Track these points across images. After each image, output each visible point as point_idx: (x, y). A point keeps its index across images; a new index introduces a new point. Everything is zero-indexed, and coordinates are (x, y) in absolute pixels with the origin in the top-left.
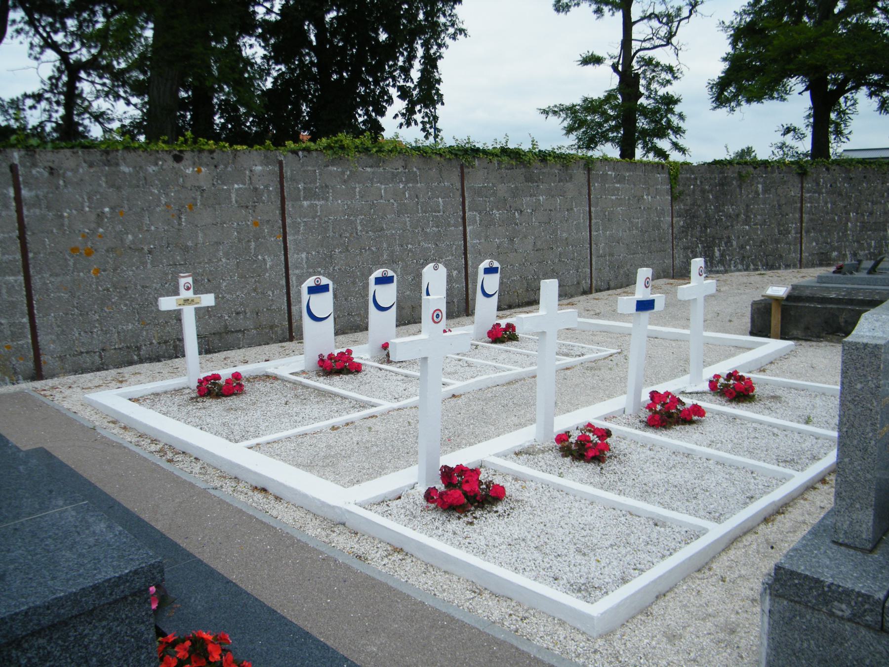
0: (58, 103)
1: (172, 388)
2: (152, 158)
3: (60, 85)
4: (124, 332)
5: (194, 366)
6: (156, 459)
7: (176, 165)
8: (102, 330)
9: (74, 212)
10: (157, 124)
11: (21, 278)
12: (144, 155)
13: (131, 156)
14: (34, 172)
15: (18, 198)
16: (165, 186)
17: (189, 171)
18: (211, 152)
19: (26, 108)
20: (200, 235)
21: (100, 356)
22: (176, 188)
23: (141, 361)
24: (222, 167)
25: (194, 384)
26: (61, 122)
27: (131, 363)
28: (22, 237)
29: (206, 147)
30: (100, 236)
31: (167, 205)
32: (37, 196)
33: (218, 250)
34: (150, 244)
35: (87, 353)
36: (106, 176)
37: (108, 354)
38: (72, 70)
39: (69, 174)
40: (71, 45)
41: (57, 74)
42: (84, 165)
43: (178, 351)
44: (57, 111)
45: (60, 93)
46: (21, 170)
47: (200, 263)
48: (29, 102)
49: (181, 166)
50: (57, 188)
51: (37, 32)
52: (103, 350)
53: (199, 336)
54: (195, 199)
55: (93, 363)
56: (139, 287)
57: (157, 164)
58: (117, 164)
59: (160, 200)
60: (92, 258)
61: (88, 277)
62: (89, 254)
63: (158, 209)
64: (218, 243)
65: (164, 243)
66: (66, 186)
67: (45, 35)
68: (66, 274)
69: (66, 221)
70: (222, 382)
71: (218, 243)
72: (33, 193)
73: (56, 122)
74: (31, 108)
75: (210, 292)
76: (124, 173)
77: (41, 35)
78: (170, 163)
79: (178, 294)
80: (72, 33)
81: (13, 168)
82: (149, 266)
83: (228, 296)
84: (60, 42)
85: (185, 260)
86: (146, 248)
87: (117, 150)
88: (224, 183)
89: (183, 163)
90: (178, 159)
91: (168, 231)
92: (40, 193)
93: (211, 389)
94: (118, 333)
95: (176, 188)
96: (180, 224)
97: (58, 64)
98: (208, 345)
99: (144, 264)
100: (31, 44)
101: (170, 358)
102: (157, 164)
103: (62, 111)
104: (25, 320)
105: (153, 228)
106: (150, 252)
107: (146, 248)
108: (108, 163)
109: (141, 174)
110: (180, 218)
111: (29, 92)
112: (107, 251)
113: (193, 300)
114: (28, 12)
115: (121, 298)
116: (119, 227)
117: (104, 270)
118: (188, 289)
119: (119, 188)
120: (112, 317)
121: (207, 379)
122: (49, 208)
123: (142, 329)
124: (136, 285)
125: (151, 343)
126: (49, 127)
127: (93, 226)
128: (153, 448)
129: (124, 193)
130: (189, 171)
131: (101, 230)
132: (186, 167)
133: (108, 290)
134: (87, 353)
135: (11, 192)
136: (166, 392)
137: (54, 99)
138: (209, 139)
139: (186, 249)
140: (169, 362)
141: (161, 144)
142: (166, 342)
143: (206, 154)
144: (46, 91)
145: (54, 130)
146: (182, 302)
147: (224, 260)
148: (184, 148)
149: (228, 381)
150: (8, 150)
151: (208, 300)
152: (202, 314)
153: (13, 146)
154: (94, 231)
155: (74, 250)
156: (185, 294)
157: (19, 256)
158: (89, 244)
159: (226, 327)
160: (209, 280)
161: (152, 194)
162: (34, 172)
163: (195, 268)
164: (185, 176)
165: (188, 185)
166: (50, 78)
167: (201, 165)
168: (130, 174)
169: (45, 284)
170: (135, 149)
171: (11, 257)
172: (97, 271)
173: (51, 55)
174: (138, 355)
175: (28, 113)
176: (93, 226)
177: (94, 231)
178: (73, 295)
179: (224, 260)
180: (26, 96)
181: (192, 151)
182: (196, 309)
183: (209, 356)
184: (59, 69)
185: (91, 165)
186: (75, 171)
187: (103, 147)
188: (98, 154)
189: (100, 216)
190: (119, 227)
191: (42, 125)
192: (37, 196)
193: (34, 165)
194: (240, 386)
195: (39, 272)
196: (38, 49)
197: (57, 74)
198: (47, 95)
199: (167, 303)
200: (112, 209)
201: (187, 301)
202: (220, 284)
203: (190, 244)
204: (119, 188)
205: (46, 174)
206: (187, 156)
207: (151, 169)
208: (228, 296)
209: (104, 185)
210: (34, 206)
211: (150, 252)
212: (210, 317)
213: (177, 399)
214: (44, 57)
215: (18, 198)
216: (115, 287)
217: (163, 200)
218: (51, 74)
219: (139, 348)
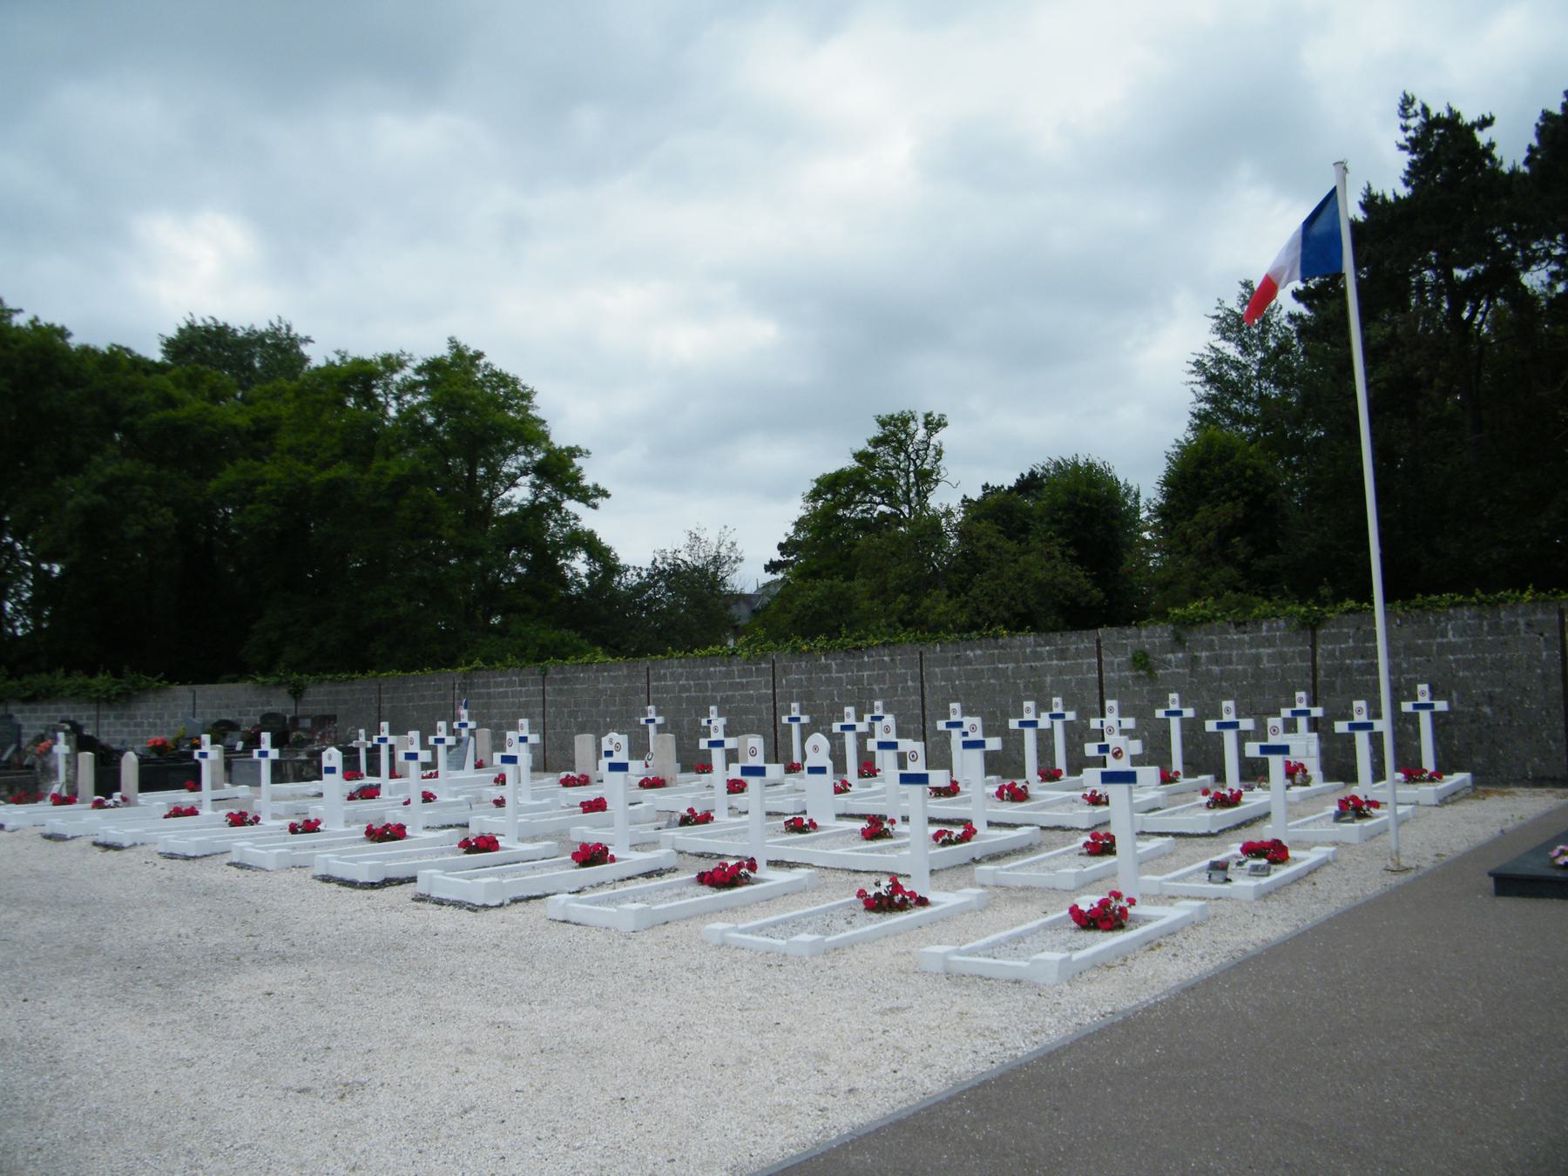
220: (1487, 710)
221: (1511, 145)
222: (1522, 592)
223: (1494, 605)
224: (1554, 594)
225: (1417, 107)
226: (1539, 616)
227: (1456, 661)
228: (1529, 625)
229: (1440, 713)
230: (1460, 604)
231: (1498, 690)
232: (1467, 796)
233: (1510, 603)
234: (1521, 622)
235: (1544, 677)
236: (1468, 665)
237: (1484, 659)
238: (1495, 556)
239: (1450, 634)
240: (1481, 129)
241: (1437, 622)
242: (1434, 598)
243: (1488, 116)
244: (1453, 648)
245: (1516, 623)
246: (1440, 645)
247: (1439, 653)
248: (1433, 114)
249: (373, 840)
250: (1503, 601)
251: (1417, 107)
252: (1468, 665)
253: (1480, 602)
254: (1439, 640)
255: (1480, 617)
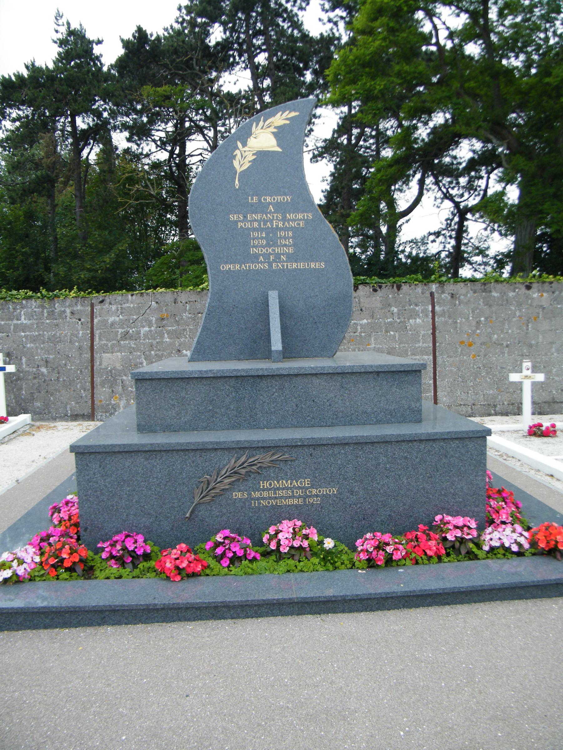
0: (451, 237)
1: (512, 429)
2: (512, 287)
3: (453, 223)
5: (528, 419)
6: (498, 458)
7: (527, 292)
9: (464, 320)
10: (521, 260)
11: (431, 357)
12: (507, 285)
13: (499, 286)
14: (443, 296)
15: (433, 311)
16: (519, 305)
17: (535, 295)
18: (551, 283)
19: (429, 242)
20: (540, 337)
21: (472, 408)
22: (527, 306)
23: (496, 414)
24: (557, 293)
25: (526, 428)
26: (452, 251)
27: (490, 415)
28: (434, 334)
29: (547, 280)
31: (520, 317)
32: (443, 310)
33: (551, 348)
34: (507, 341)
36: (483, 298)
37: (476, 407)
38: (462, 213)
39: (462, 297)
40: (462, 196)
41: (451, 217)
42: (471, 292)
43: (518, 411)
44: (449, 243)
45: (452, 230)
46: (436, 295)
48: (432, 238)
49: (530, 292)
50: (455, 305)
51: (440, 189)
53: (534, 403)
54: (538, 313)
56: (499, 368)
57: (514, 291)
58: (490, 291)
59: (515, 314)
60: (472, 348)
62: (470, 345)
63: (514, 319)
64: (552, 343)
65: (516, 341)
66: (459, 304)
67: (445, 190)
68: (456, 357)
69: (459, 325)
70: (543, 428)
71: (552, 343)
72: (441, 308)
73: (448, 251)
74: (432, 242)
76: (494, 297)
77: (443, 192)
78: (523, 290)
79: (521, 372)
80: (463, 187)
81: (432, 294)
82: (506, 355)
83: (557, 378)
84: (454, 194)
86: (505, 344)
87: (491, 283)
88: (558, 304)
89: (532, 290)
90: (528, 287)
92: (446, 309)
93: (536, 432)
95: (527, 306)
96: (527, 329)
97: (452, 209)
99: (503, 353)
100: (436, 197)
101: (515, 414)
102: (514, 291)
103: (453, 242)
104: (432, 382)
105: (510, 331)
106: (507, 346)
107: (505, 344)
108: (485, 291)
109: (505, 298)
110: (528, 326)
111: (432, 231)
112: (481, 344)
114: (436, 177)
115: (487, 373)
116: (489, 330)
118: (528, 369)
119: (490, 306)
121: (535, 426)
122: (449, 317)
123: (498, 394)
124: (497, 366)
125: (503, 404)
126: (443, 255)
127: (474, 328)
128: (497, 453)
129: (494, 309)
130: (535, 295)
131: (478, 331)
132: (534, 293)
133: (480, 368)
135: (430, 308)
136: (508, 431)
137: (448, 234)
138: (550, 275)
139: (531, 346)
140: (514, 417)
141: (518, 279)
142: (513, 404)
143: (547, 284)
144: (444, 230)
145: (447, 256)
147: (555, 354)
148: (533, 280)
149: (547, 428)
150: (430, 284)
151: (540, 377)
152: (535, 385)
153: (433, 281)
154: (474, 332)
155: (462, 342)
156: (526, 372)
157: (431, 345)
158: (471, 340)
159: (553, 398)
160: (544, 367)
161: (511, 310)
162: (443, 296)
163: (535, 358)
164: (533, 299)
165: (534, 304)
166: (447, 220)
167: (543, 291)
168: (498, 297)
169: (444, 362)
170: (502, 282)
171: (427, 345)
172: (474, 356)
173: (448, 204)
174: (495, 410)
175: (430, 245)
176: (474, 328)
177: (474, 332)
178: (459, 370)
179: (555, 354)
180: (430, 234)
181: (538, 282)
183: (540, 416)
184: (452, 213)
185: (475, 292)
186: (465, 295)
187: (483, 281)
188: (480, 285)
189: (478, 323)
190: (489, 330)
191: (439, 253)
192: (443, 310)
193: (443, 292)
194: (555, 432)
195: (441, 355)
196: (439, 201)
197: (451, 217)
198: (443, 232)
199: (514, 377)
200: (486, 318)
202: (552, 370)
203: (533, 342)
204: (490, 306)
205: (449, 297)
206: (535, 286)
207: (511, 294)
208: (557, 378)
209: (482, 304)
210: (441, 316)
211: (507, 346)
212: (543, 391)
213: (515, 435)
214: (443, 206)
215: (433, 311)
216: (484, 366)
217: (518, 314)
218: (447, 217)
219: (495, 406)
220: (44, 370)
221: (109, 54)
222: (70, 292)
223: (51, 299)
224: (89, 293)
225: (64, 20)
226: (79, 307)
227: (26, 336)
228: (72, 313)
229: (10, 373)
230: (30, 297)
231: (51, 357)
232: (24, 434)
233: (62, 298)
234: (68, 311)
235: (80, 348)
236: (34, 340)
237: (43, 335)
238: (82, 276)
239: (23, 317)
240: (97, 44)
241: (15, 309)
242: (14, 292)
243: (101, 39)
244: (24, 328)
245: (64, 312)
246: (16, 325)
247: (15, 331)
248: (72, 28)
249: (522, 411)
250: (57, 296)
251: (64, 20)
252: (34, 340)
253: (43, 297)
254: (15, 322)
255: (43, 307)
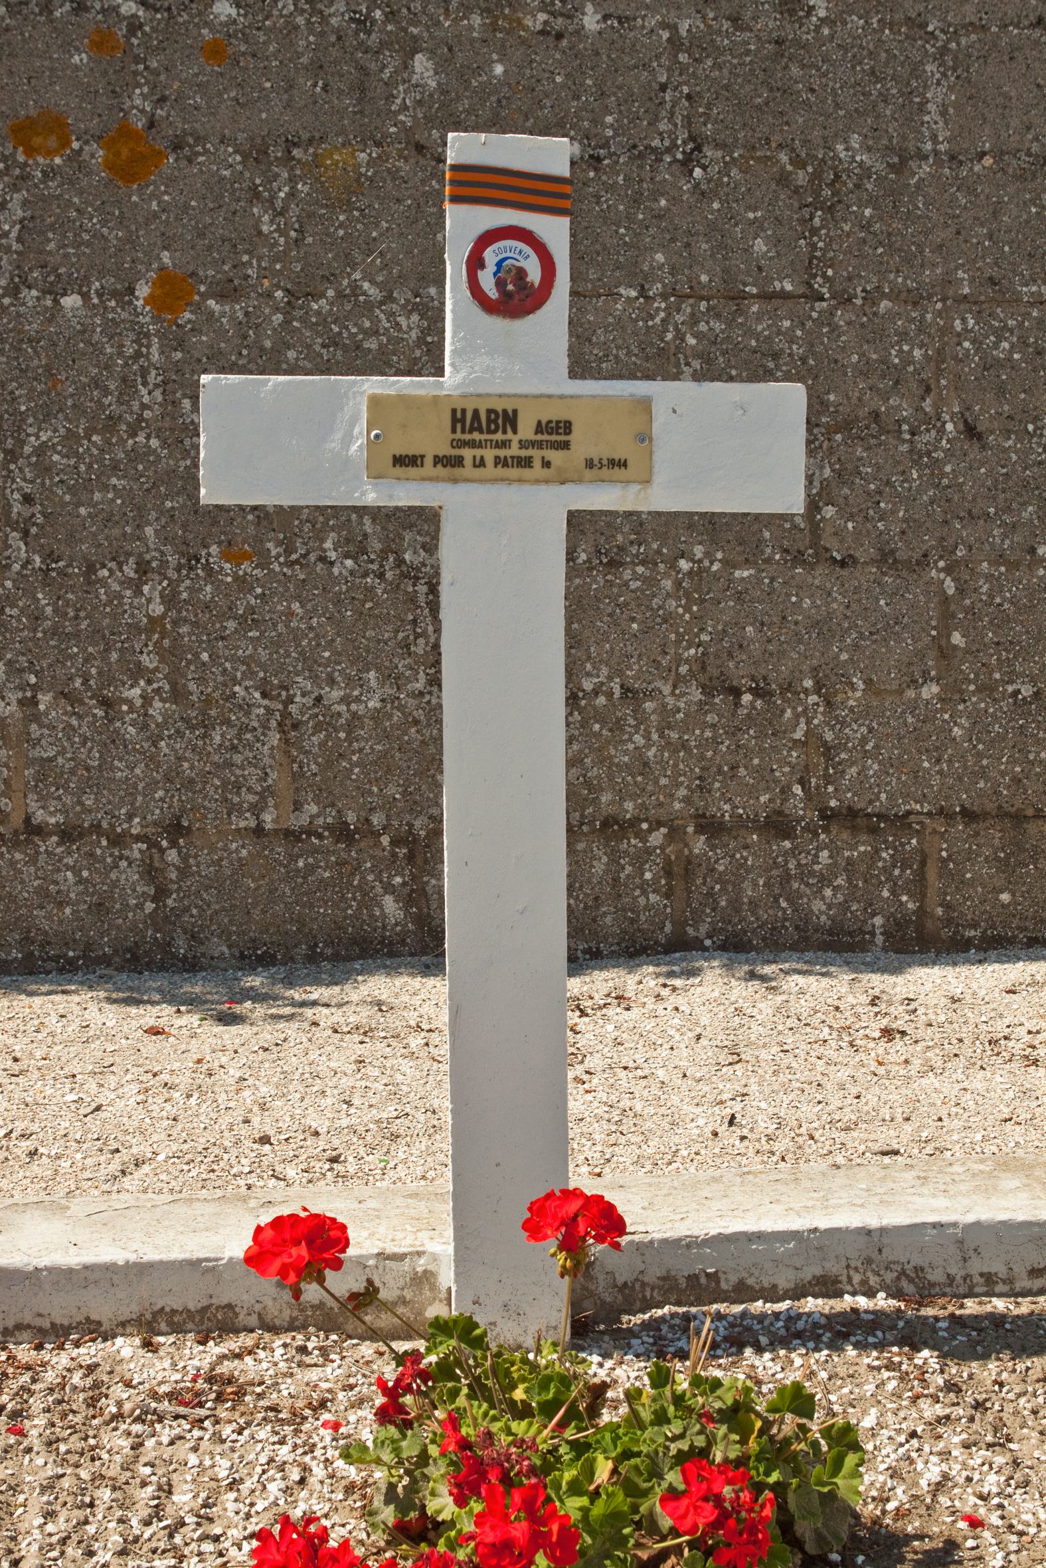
4: (327, 724)
8: (178, 694)
30: (215, 51)
35: (67, 834)
47: (916, 299)
52: (176, 830)
55: (100, 908)
60: (152, 197)
61: (112, 330)
62: (132, 158)
65: (668, 131)
75: (758, 367)
79: (429, 360)
85: (810, 266)
91: (700, 46)
94: (289, 725)
98: (919, 886)
113: (557, 432)
117: (227, 291)
118: (515, 299)
120: (250, 620)
134: (67, 834)
139: (827, 192)
146: (435, 439)
151: (733, 447)
160: (971, 431)
182: (577, 521)
199: (279, 438)
201: (484, 434)
203: (852, 150)
212: (952, 695)
